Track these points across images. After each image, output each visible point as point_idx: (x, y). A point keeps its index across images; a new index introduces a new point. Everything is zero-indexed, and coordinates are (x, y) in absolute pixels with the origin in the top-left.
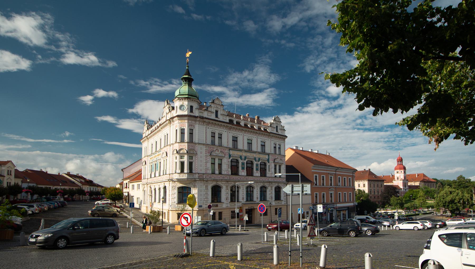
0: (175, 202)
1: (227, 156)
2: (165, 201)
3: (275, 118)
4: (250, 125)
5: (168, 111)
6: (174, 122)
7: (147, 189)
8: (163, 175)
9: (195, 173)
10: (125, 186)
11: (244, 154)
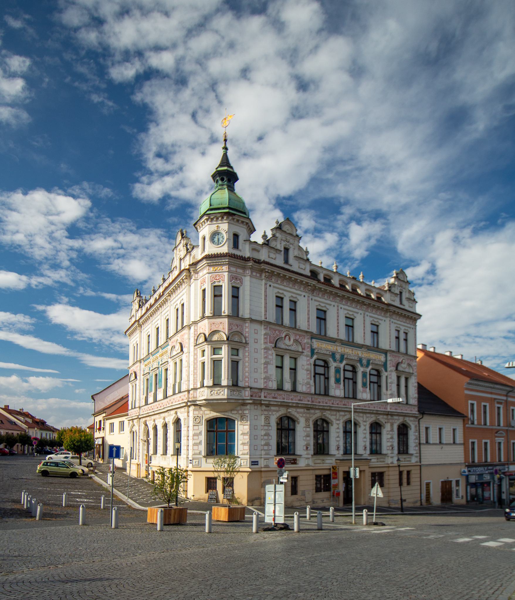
0: (200, 453)
1: (307, 352)
2: (178, 452)
3: (397, 274)
4: (350, 285)
5: (183, 252)
6: (197, 273)
7: (139, 429)
8: (174, 394)
9: (244, 388)
10: (98, 427)
11: (340, 349)
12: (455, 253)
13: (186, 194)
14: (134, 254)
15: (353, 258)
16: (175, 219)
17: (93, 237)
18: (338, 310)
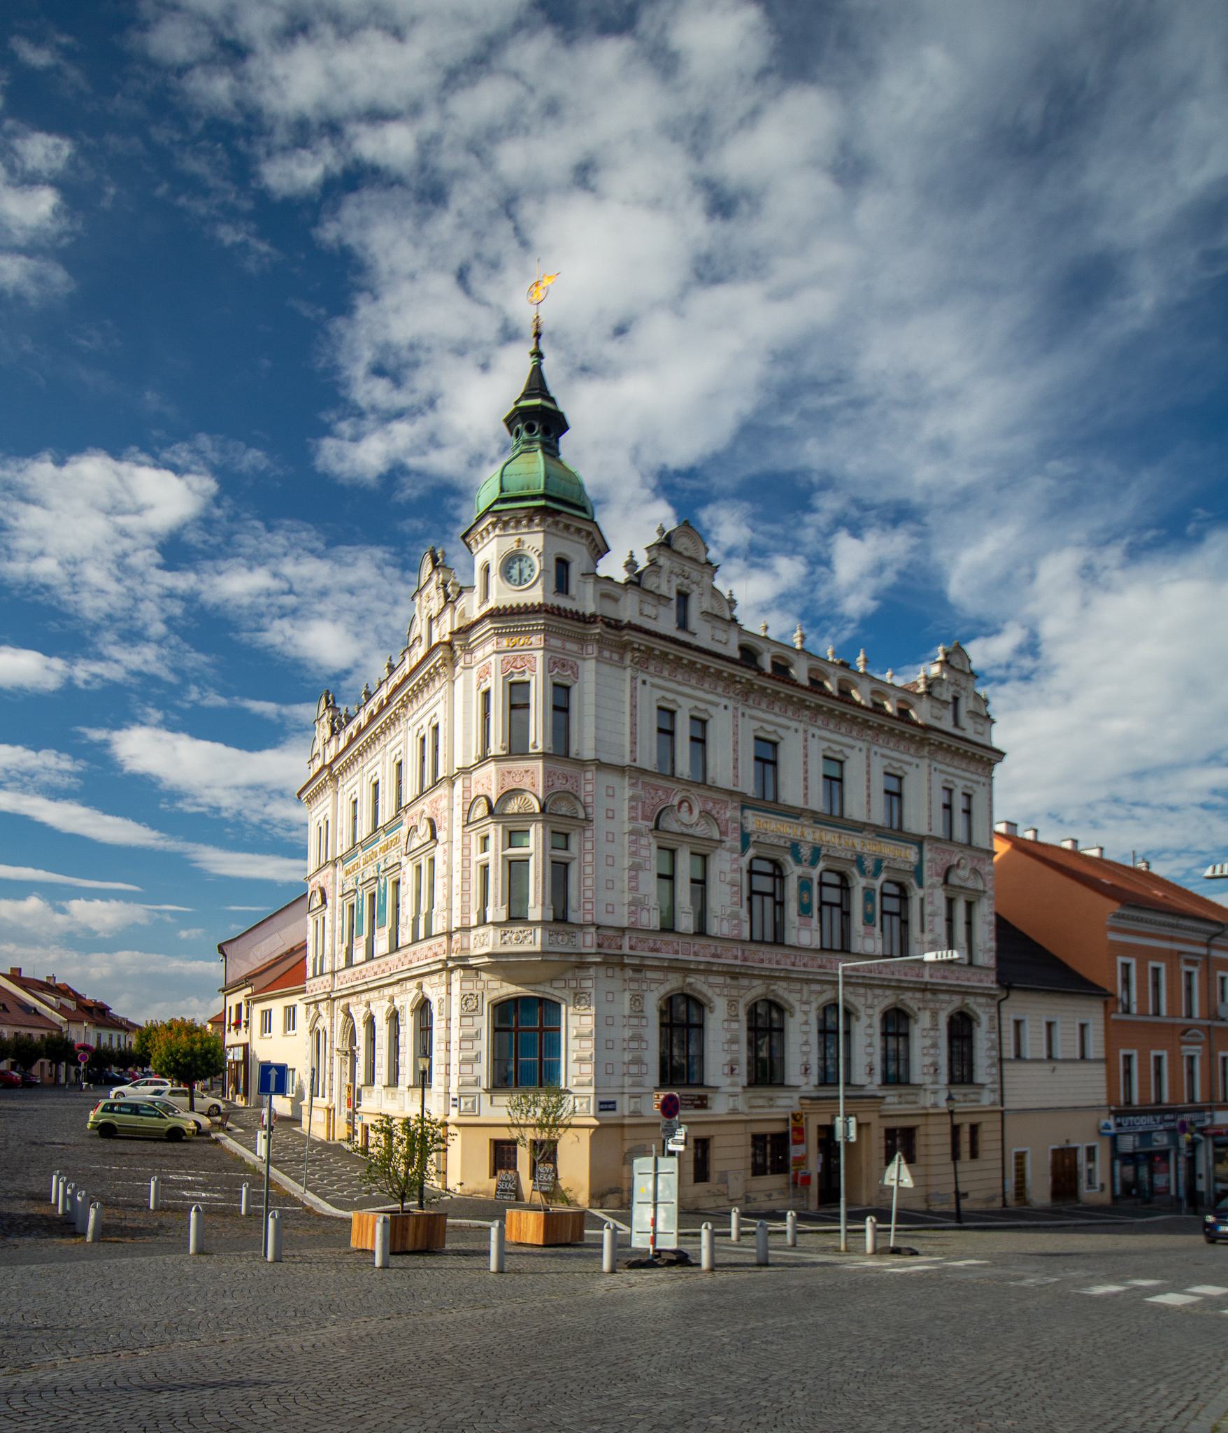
0: (477, 1083)
1: (733, 840)
2: (423, 1079)
3: (947, 654)
4: (835, 680)
5: (436, 603)
7: (332, 1025)
8: (415, 940)
9: (581, 926)
10: (233, 1020)
11: (810, 835)
12: (1085, 604)
13: (444, 462)
14: (319, 607)
15: (842, 617)
16: (417, 524)
17: (223, 565)
18: (806, 740)
